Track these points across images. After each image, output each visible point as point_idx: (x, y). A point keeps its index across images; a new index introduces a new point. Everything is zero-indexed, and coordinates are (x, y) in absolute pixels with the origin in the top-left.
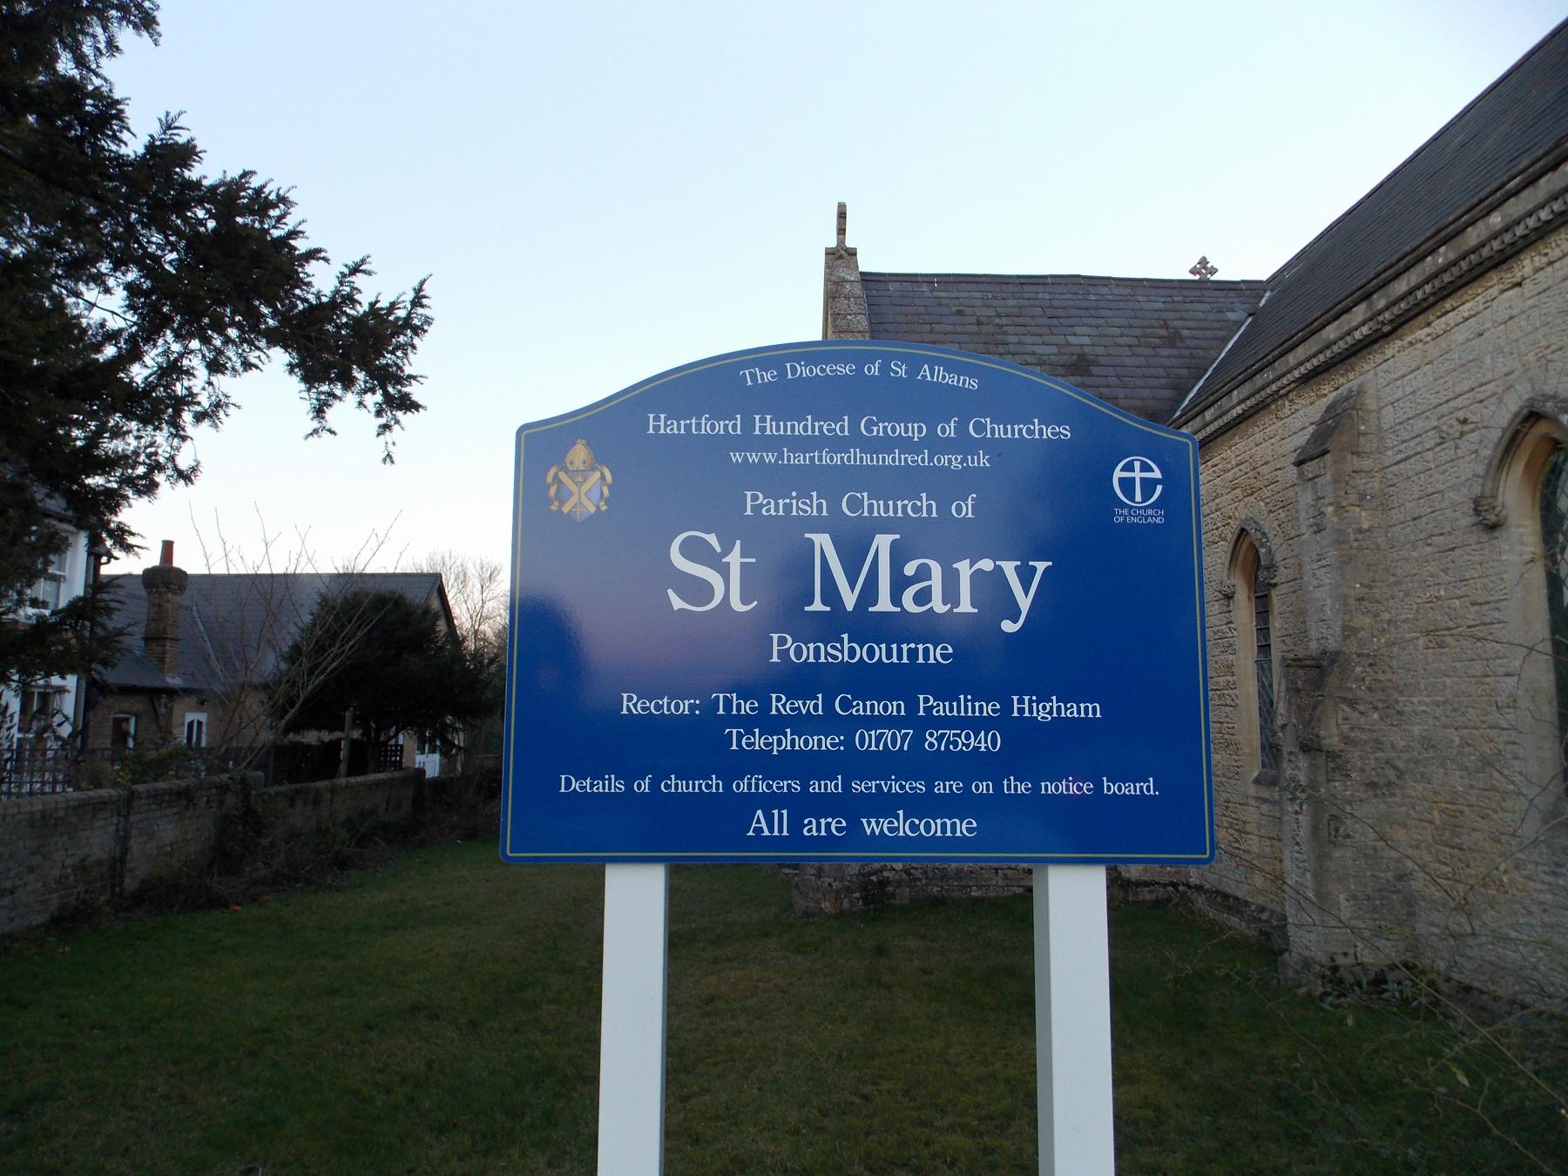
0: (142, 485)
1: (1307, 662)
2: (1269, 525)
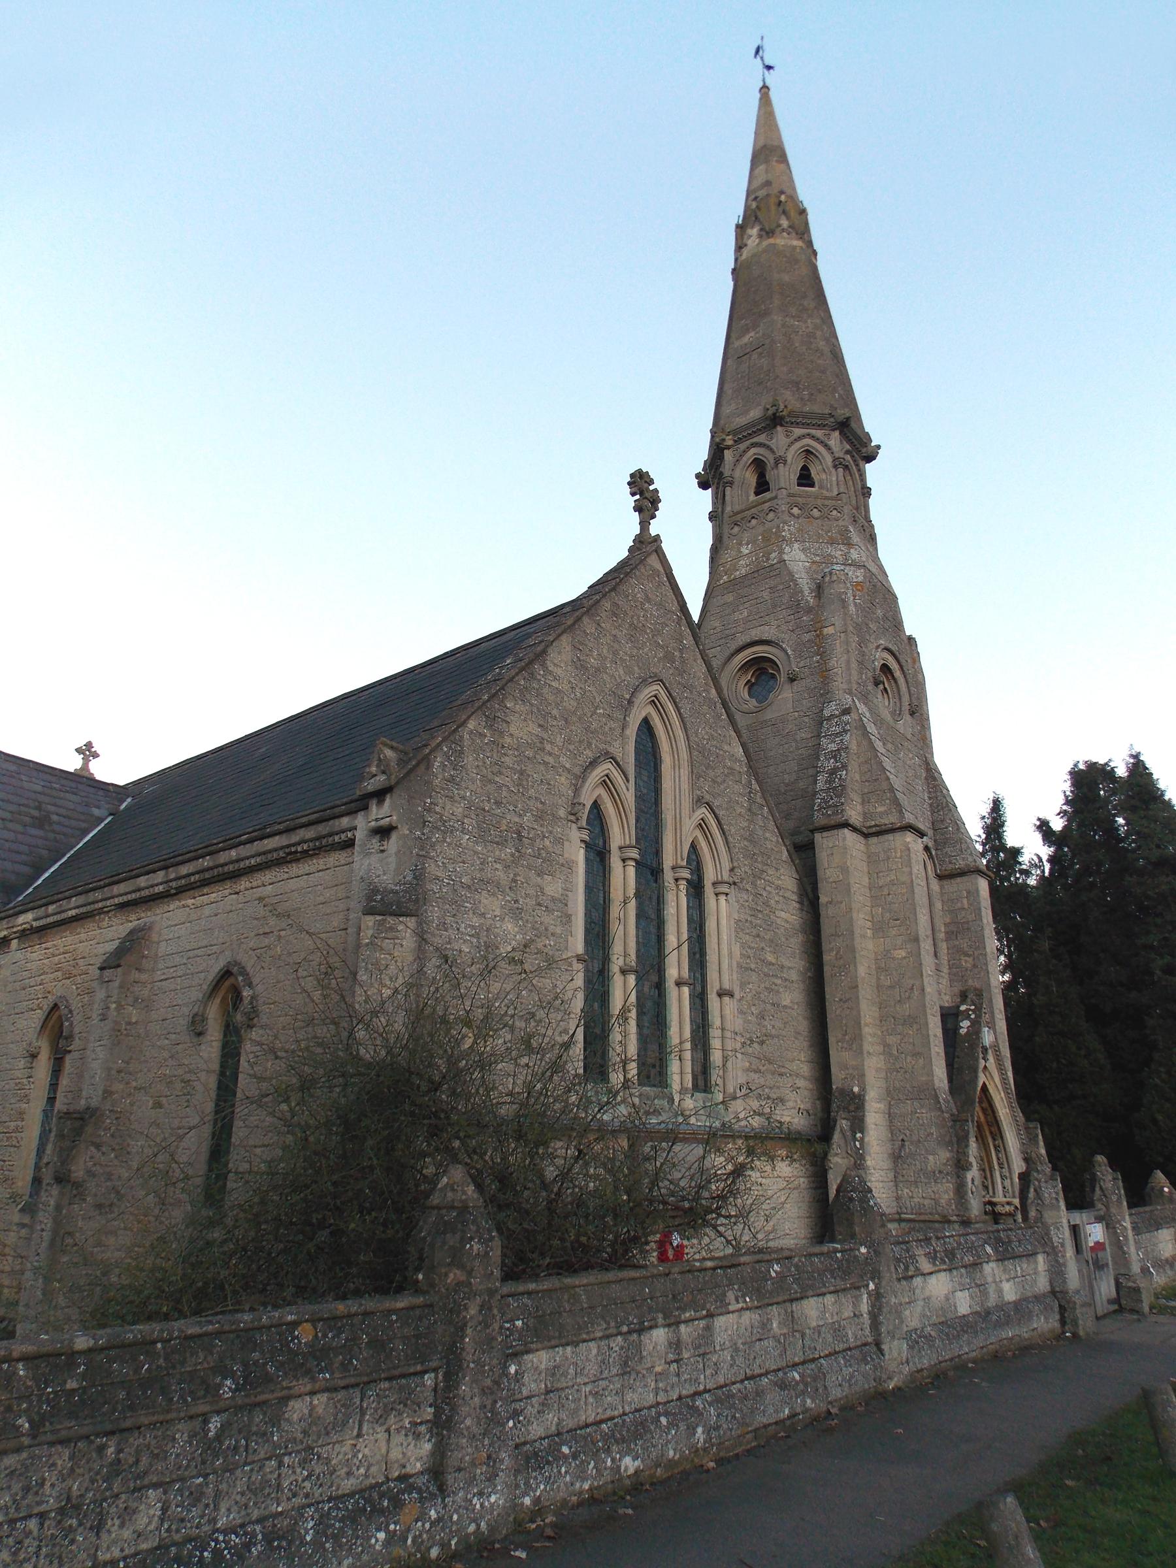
1: (75, 1115)
2: (75, 1004)
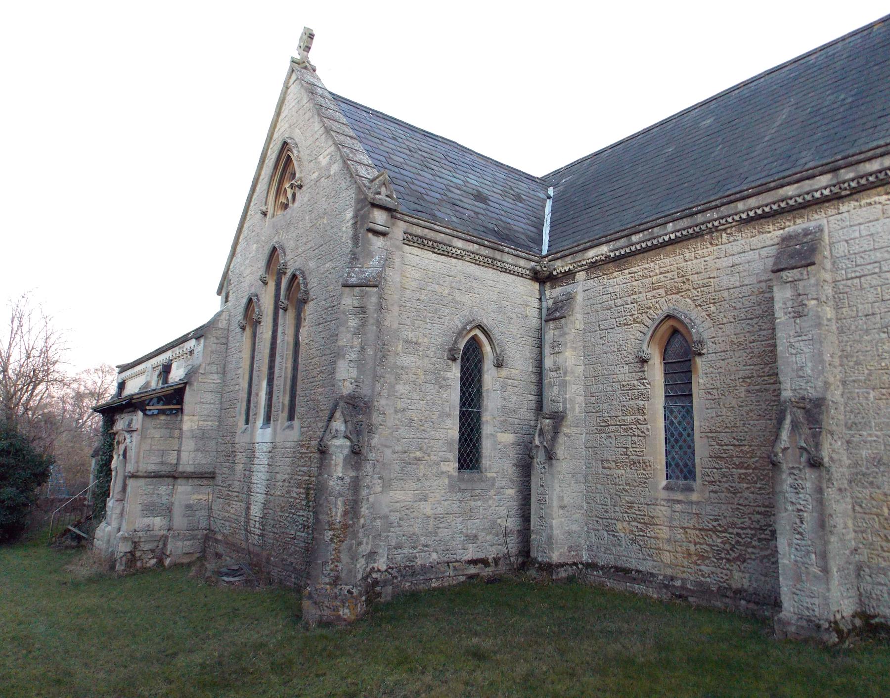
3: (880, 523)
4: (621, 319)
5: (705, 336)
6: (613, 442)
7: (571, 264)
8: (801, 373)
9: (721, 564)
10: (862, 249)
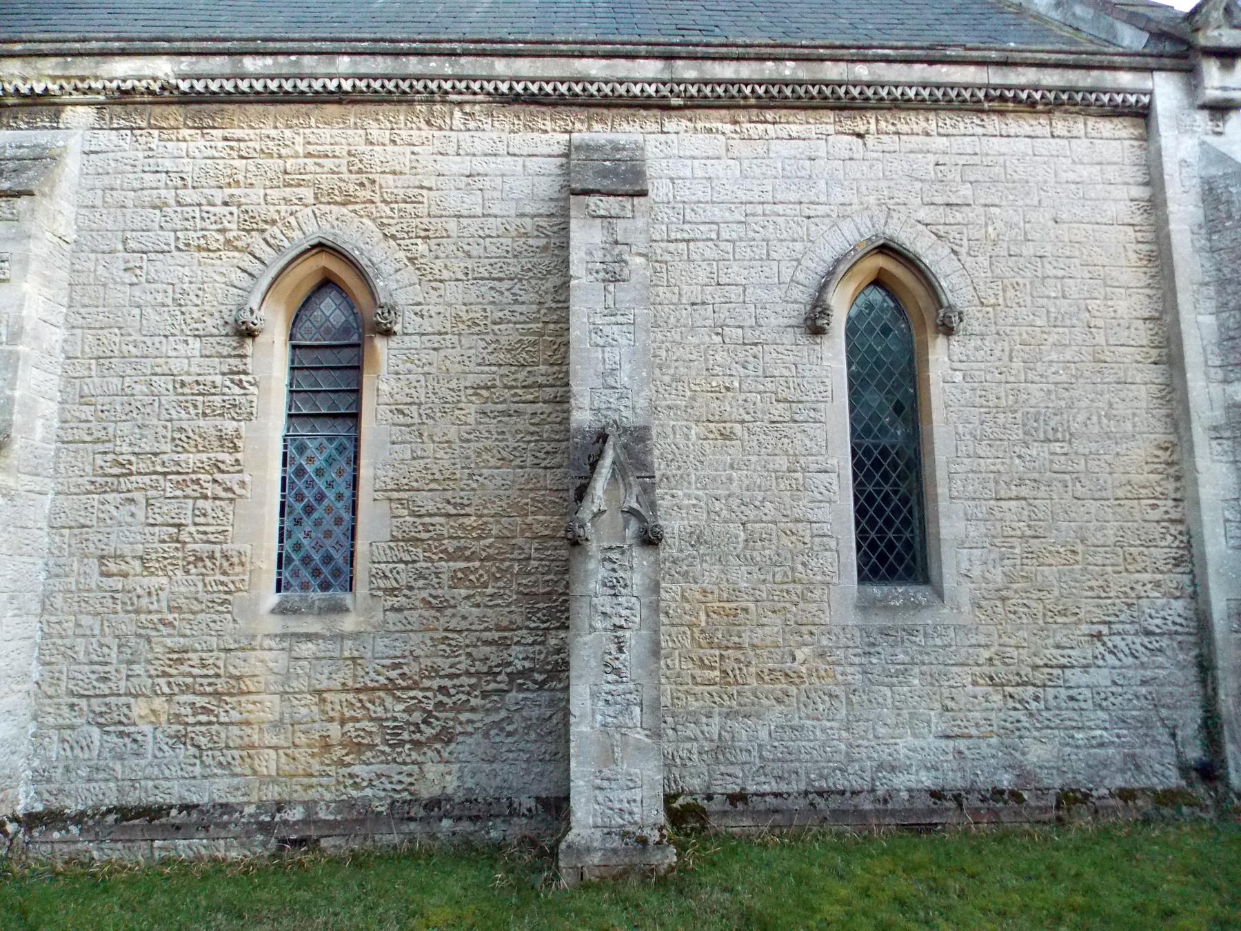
0: (1134, 718)
3: (693, 638)
4: (191, 234)
5: (401, 298)
6: (141, 515)
7: (54, 78)
8: (611, 381)
9: (400, 754)
10: (695, 198)
